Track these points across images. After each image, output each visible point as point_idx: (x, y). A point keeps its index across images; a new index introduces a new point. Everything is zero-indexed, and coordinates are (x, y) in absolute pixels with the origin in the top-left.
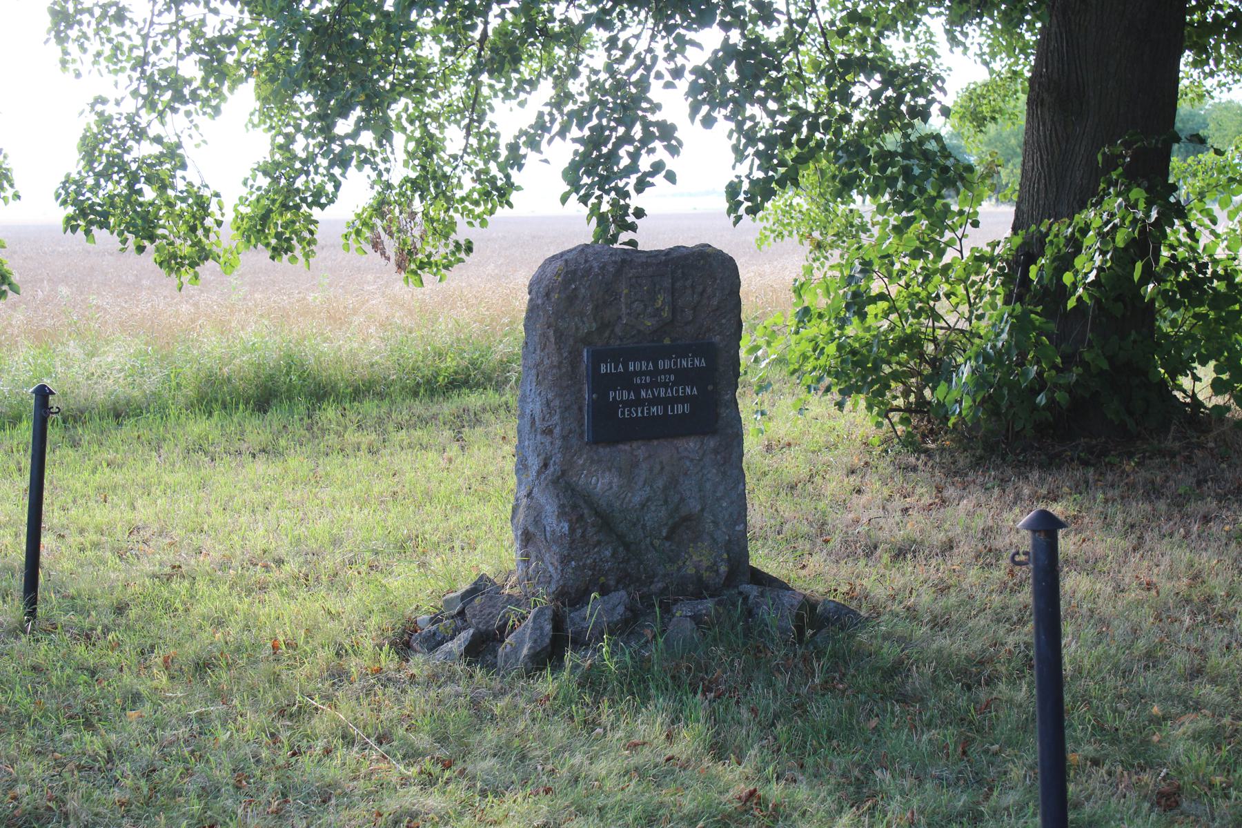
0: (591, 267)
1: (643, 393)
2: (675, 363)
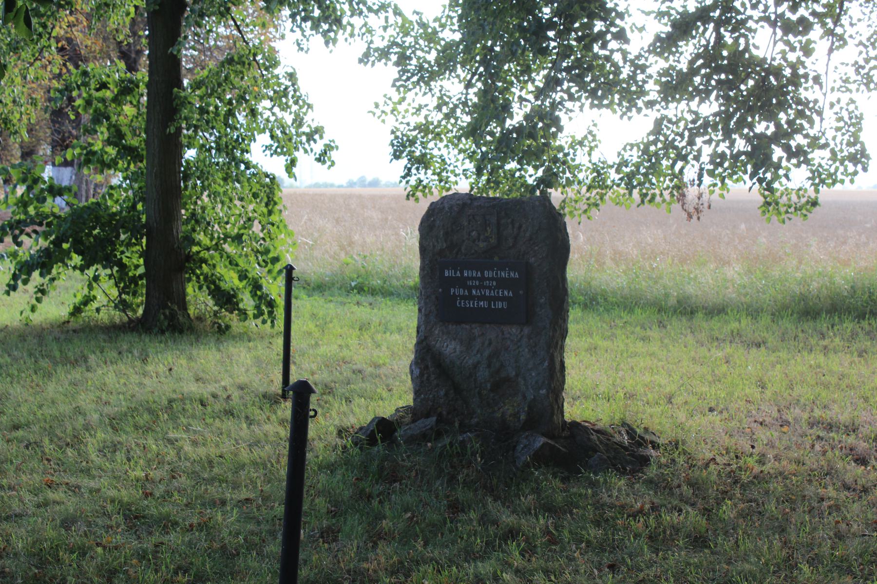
0: (444, 207)
1: (474, 292)
2: (497, 274)
